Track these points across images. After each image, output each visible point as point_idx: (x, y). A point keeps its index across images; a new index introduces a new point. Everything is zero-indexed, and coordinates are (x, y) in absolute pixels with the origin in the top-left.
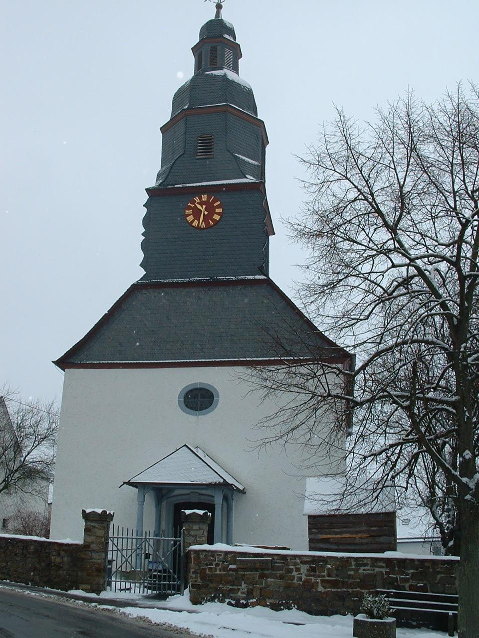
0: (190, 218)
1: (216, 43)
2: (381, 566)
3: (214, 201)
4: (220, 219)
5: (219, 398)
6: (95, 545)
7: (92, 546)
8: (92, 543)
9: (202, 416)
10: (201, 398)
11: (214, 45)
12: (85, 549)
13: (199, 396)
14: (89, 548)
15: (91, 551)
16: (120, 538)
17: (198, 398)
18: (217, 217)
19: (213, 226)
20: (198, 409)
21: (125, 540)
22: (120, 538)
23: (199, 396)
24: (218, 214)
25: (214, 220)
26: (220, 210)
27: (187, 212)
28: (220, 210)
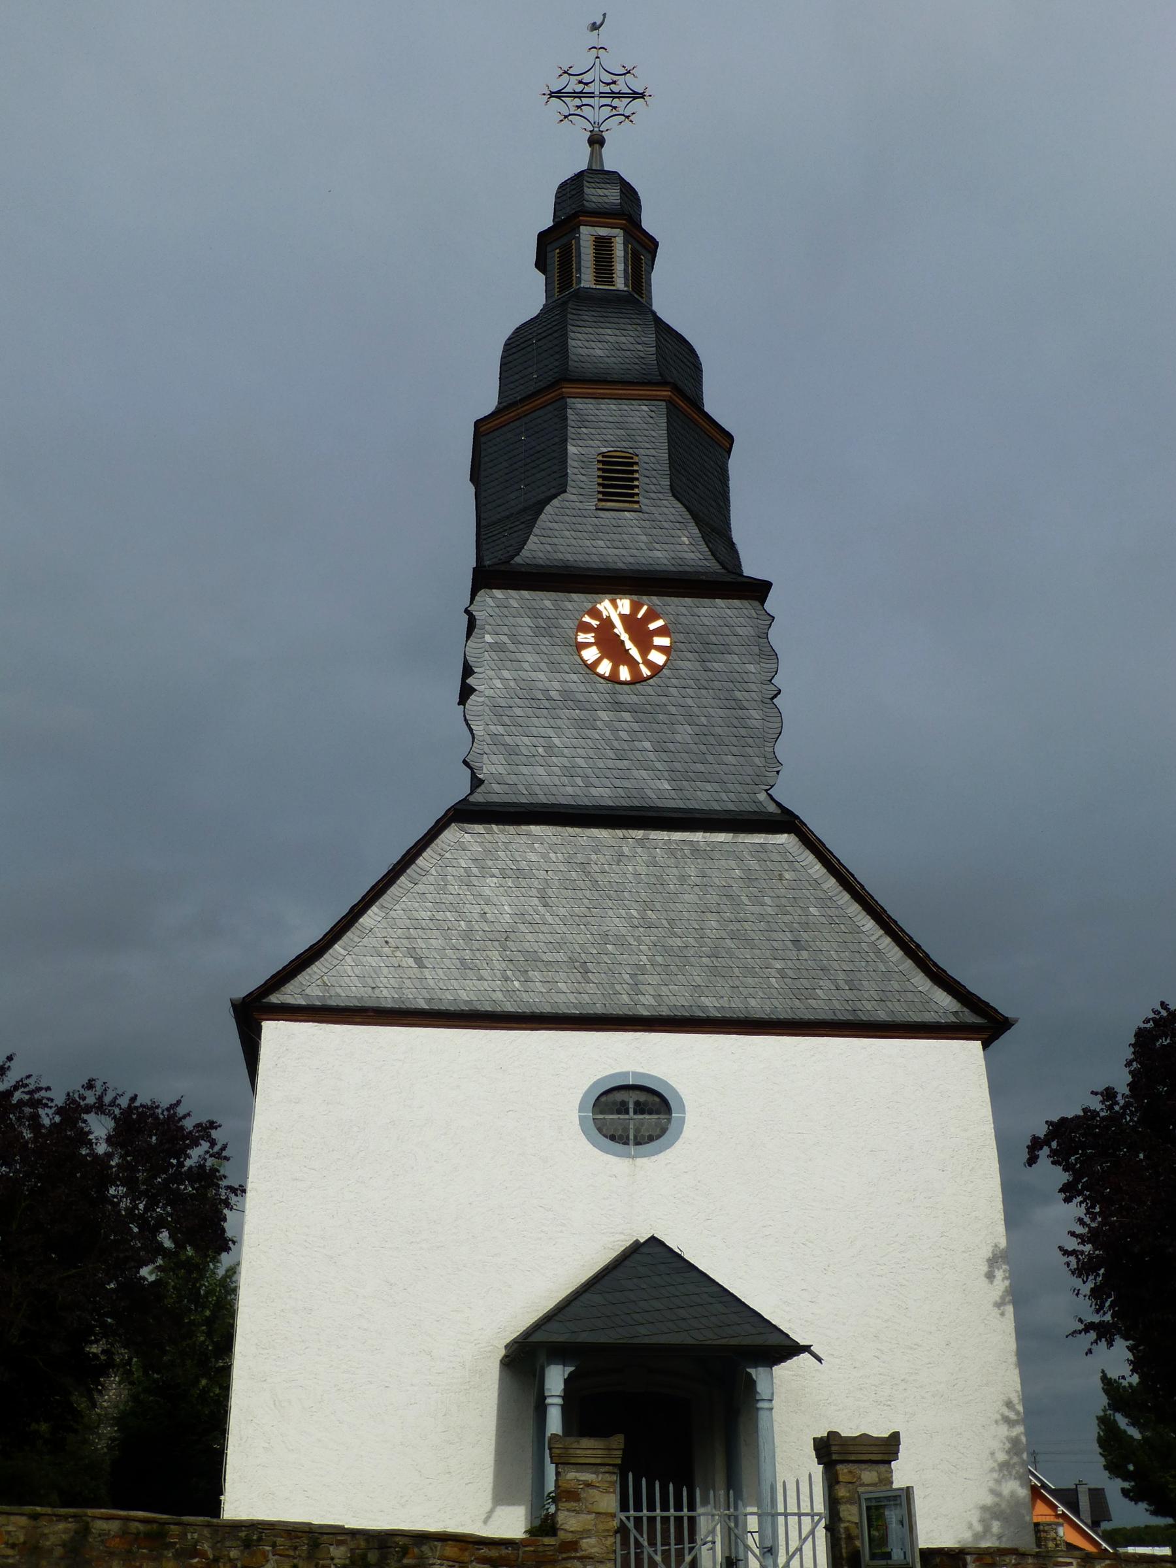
0: (590, 655)
1: (1103, 1371)
2: (561, 255)
3: (652, 615)
4: (665, 664)
5: (628, 1073)
6: (593, 1541)
7: (585, 1543)
8: (586, 1533)
9: (645, 1160)
10: (635, 1113)
11: (603, 232)
12: (564, 1556)
13: (631, 1106)
14: (576, 1551)
15: (580, 1559)
16: (794, 1514)
17: (627, 1112)
18: (658, 658)
19: (649, 678)
20: (631, 1142)
21: (793, 1520)
22: (794, 1514)
23: (631, 1106)
24: (661, 649)
25: (650, 664)
26: (665, 641)
27: (582, 637)
28: (665, 641)
